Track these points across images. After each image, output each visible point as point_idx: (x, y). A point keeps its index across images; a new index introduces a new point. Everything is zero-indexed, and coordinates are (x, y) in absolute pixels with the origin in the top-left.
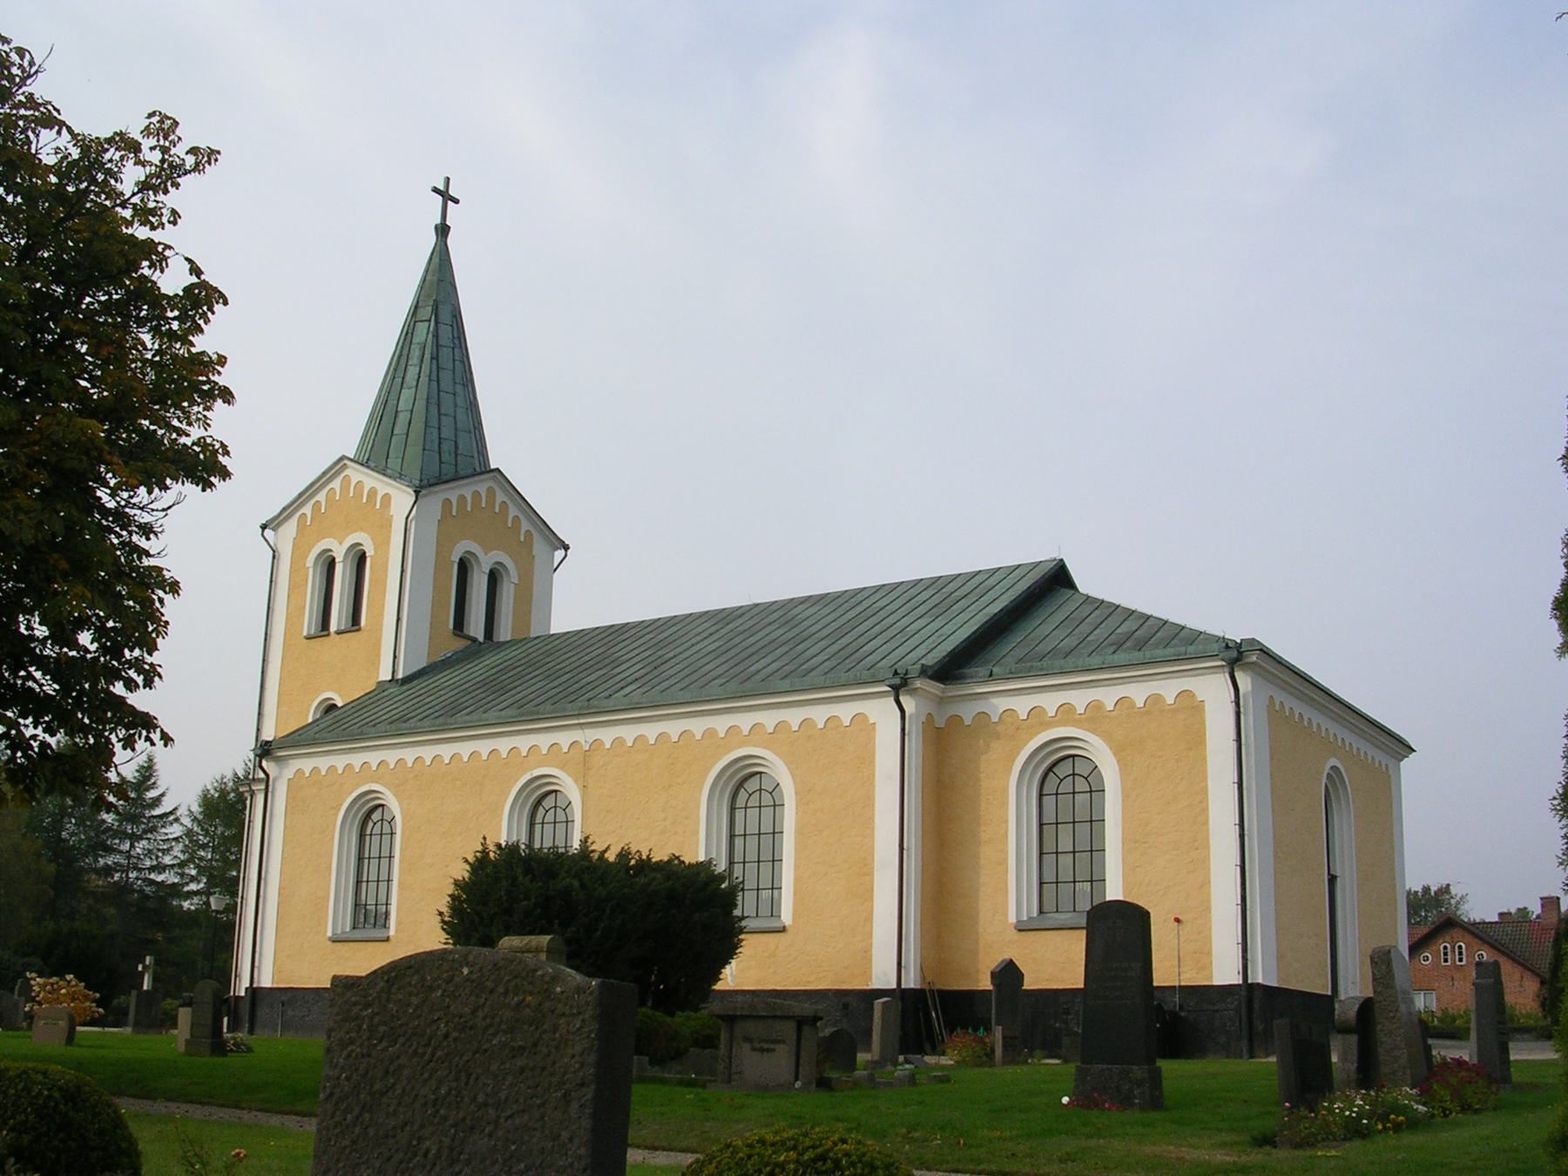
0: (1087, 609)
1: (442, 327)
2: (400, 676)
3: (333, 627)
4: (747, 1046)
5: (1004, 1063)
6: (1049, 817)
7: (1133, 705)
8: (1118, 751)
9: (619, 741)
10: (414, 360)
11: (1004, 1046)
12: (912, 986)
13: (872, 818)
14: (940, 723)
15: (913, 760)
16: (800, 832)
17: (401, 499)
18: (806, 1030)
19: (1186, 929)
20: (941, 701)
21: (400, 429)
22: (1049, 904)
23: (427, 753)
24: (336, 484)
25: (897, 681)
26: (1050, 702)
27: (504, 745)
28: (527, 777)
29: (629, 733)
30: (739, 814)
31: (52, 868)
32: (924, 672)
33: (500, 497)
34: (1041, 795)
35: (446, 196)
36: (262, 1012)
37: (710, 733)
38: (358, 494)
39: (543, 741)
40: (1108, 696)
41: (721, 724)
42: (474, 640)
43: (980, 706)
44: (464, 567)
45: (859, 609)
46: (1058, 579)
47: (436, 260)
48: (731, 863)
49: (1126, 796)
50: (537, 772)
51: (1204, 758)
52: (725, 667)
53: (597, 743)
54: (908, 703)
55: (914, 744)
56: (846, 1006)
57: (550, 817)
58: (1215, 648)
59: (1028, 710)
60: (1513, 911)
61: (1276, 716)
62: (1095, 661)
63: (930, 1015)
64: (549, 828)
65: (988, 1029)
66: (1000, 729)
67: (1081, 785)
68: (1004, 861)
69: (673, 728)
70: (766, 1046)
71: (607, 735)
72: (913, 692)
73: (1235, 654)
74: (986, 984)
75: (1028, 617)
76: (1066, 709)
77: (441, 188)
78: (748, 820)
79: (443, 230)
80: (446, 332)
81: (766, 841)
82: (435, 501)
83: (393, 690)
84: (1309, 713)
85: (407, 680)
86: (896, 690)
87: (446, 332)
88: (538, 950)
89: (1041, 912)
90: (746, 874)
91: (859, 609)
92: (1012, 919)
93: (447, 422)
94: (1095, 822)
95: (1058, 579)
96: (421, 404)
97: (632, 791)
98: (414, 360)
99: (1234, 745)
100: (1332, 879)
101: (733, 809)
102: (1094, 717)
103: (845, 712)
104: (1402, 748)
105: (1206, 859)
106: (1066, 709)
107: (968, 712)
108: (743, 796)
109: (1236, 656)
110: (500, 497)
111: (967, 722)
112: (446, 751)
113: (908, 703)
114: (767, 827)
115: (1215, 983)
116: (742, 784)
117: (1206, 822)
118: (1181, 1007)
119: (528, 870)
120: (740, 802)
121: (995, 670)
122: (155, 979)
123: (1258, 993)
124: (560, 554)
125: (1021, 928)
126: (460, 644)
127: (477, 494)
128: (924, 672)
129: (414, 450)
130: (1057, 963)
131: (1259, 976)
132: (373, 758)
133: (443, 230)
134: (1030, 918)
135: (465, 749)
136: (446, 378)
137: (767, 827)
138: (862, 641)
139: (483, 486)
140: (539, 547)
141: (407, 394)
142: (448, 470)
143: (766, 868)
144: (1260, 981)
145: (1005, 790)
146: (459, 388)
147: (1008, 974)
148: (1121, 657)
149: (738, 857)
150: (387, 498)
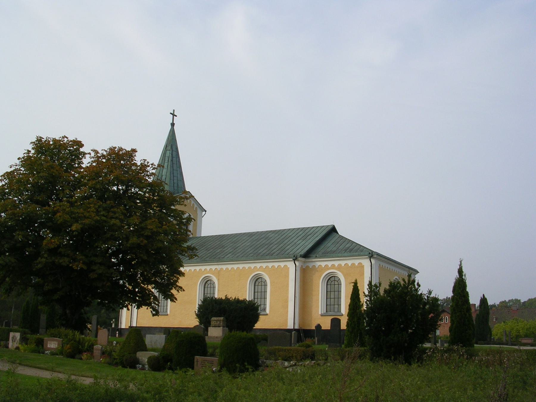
0: (339, 239)
6: (329, 290)
9: (227, 269)
15: (298, 277)
16: (271, 292)
20: (305, 262)
22: (328, 310)
26: (330, 264)
27: (198, 268)
28: (204, 276)
30: (256, 287)
34: (327, 285)
35: (174, 115)
37: (250, 268)
39: (208, 268)
40: (343, 263)
41: (252, 266)
45: (284, 236)
48: (254, 298)
50: (206, 275)
52: (253, 250)
53: (222, 269)
57: (209, 286)
59: (325, 265)
60: (507, 301)
61: (381, 268)
62: (340, 255)
63: (303, 334)
64: (209, 289)
65: (314, 338)
67: (336, 283)
69: (241, 266)
71: (224, 267)
72: (298, 260)
74: (314, 328)
76: (333, 266)
79: (173, 125)
81: (263, 293)
84: (389, 267)
86: (294, 260)
87: (174, 153)
88: (220, 320)
90: (258, 302)
91: (284, 236)
92: (320, 313)
93: (175, 178)
94: (339, 292)
95: (333, 230)
96: (168, 174)
99: (370, 276)
102: (339, 268)
103: (282, 264)
106: (333, 266)
107: (311, 265)
108: (257, 283)
114: (263, 290)
116: (258, 281)
119: (216, 303)
124: (204, 213)
125: (322, 315)
130: (326, 325)
133: (173, 125)
136: (175, 166)
137: (263, 290)
138: (286, 245)
143: (263, 300)
146: (178, 169)
147: (319, 327)
148: (346, 254)
149: (256, 297)
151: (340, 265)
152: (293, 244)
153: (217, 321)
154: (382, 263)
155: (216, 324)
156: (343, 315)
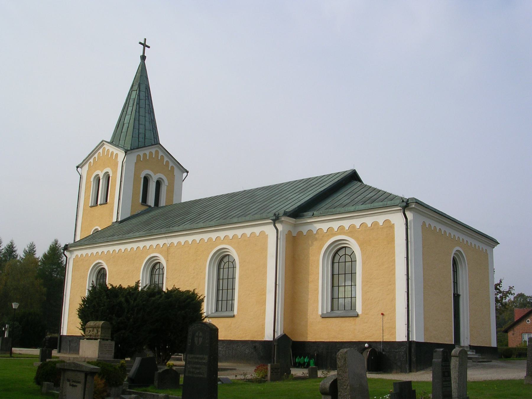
1: (141, 93)
2: (119, 220)
3: (99, 203)
4: (68, 383)
5: (272, 380)
7: (367, 226)
8: (361, 245)
10: (131, 105)
11: (271, 372)
13: (266, 273)
14: (294, 234)
17: (121, 154)
18: (89, 377)
19: (386, 318)
20: (295, 226)
21: (124, 130)
23: (117, 248)
24: (101, 151)
25: (274, 218)
26: (335, 225)
27: (141, 245)
29: (182, 240)
30: (336, 265)
31: (45, 289)
32: (286, 214)
33: (161, 154)
35: (144, 45)
36: (63, 344)
37: (210, 239)
38: (108, 154)
39: (154, 243)
40: (357, 222)
41: (213, 236)
42: (150, 206)
43: (309, 227)
44: (146, 180)
46: (353, 177)
47: (140, 68)
49: (364, 263)
50: (152, 255)
51: (394, 247)
54: (280, 226)
55: (282, 243)
56: (255, 347)
58: (398, 202)
59: (328, 228)
61: (425, 228)
66: (317, 236)
67: (348, 259)
68: (317, 289)
70: (75, 384)
71: (175, 241)
72: (281, 222)
73: (404, 204)
75: (341, 190)
76: (341, 228)
77: (143, 42)
78: (224, 273)
79: (143, 58)
80: (143, 94)
81: (230, 281)
82: (133, 156)
83: (116, 225)
85: (121, 222)
88: (98, 327)
89: (332, 309)
92: (320, 313)
93: (142, 127)
95: (353, 177)
96: (132, 121)
97: (181, 262)
98: (131, 105)
100: (457, 297)
101: (333, 263)
102: (352, 232)
103: (257, 230)
104: (494, 242)
105: (394, 290)
106: (341, 228)
107: (305, 230)
109: (406, 205)
110: (161, 154)
111: (315, 232)
112: (123, 247)
115: (397, 340)
116: (223, 261)
117: (394, 274)
118: (383, 350)
120: (336, 260)
121: (315, 213)
122: (9, 335)
124: (185, 174)
125: (323, 317)
126: (144, 208)
127: (151, 153)
128: (286, 214)
129: (129, 137)
131: (414, 338)
132: (100, 250)
133: (143, 58)
134: (327, 313)
135: (129, 247)
139: (153, 150)
140: (176, 171)
141: (128, 117)
142: (141, 144)
145: (318, 260)
146: (147, 115)
150: (117, 155)
151: (352, 227)
152: (285, 198)
153: (93, 328)
154: (428, 222)
155: (91, 333)
156: (358, 316)
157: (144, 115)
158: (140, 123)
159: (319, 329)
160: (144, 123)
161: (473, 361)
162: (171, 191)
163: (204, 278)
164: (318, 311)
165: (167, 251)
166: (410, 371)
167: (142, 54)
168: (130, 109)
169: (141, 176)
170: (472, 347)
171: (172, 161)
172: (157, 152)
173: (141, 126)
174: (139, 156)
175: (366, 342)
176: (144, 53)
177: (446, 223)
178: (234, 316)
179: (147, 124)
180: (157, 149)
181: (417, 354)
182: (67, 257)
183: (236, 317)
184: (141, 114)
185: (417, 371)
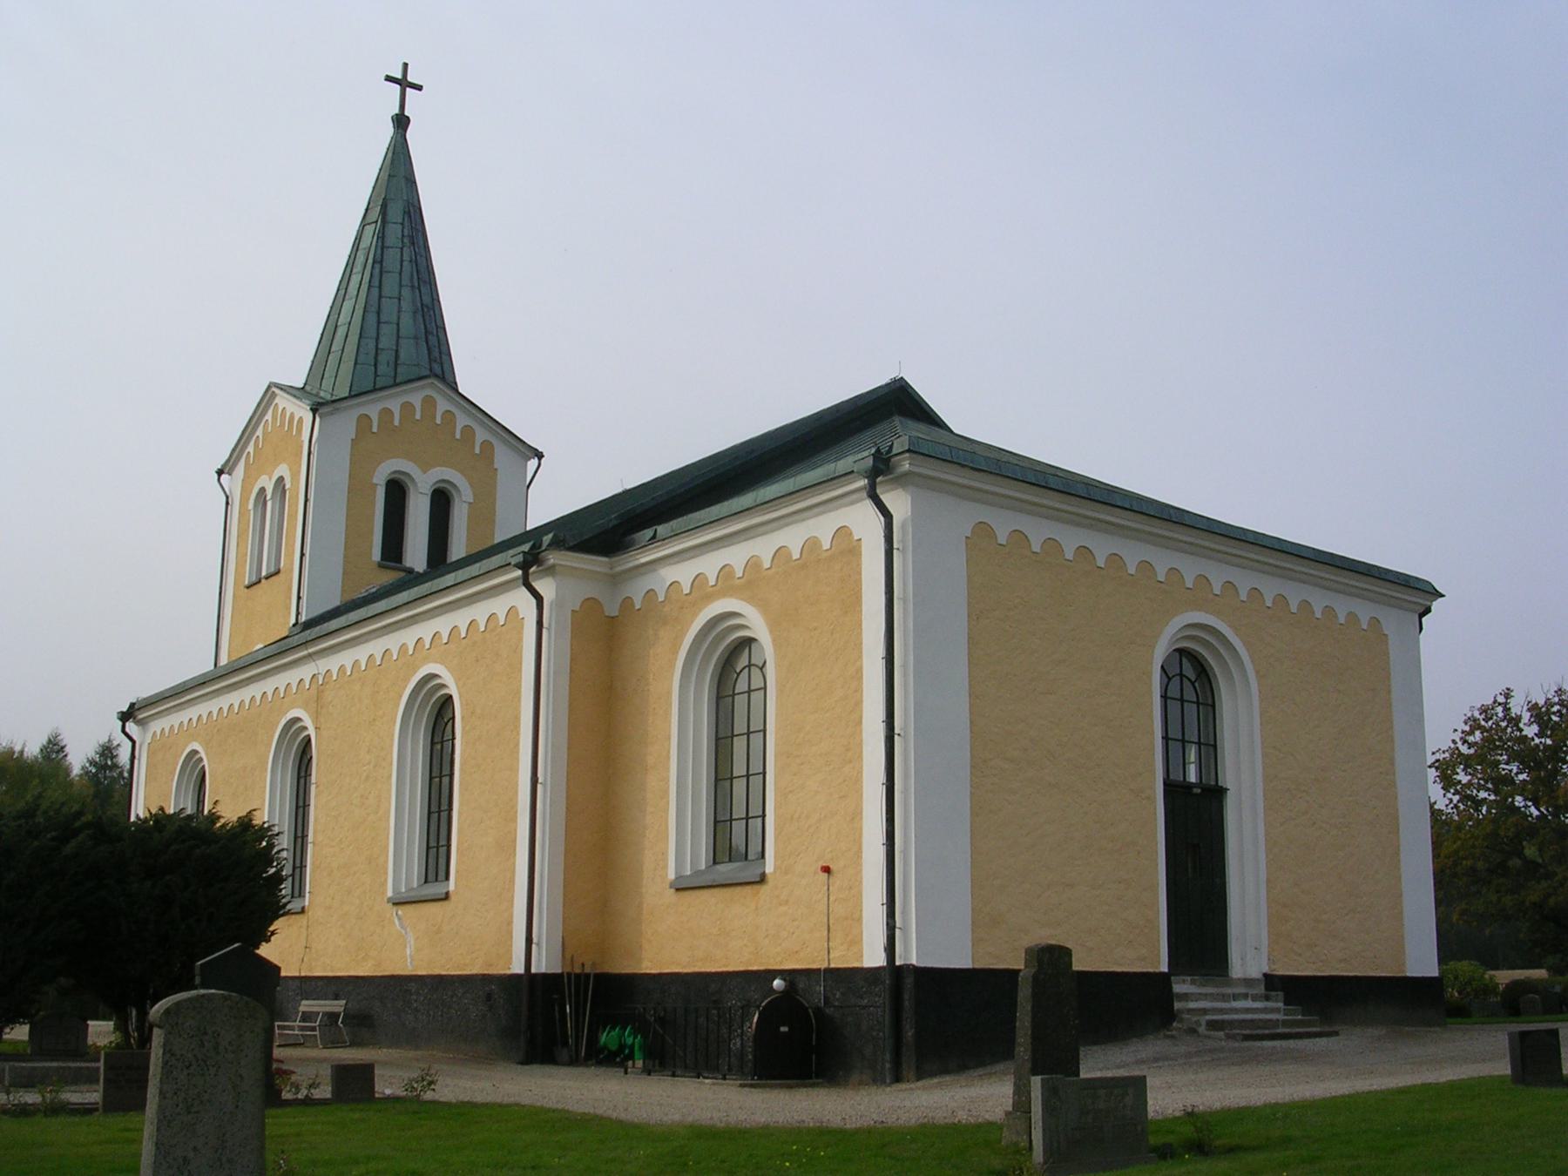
1: (390, 228)
2: (303, 618)
8: (773, 625)
12: (543, 970)
14: (612, 610)
19: (836, 881)
20: (616, 580)
28: (283, 722)
35: (403, 83)
42: (410, 571)
44: (397, 492)
46: (897, 402)
54: (545, 586)
77: (399, 76)
79: (401, 122)
80: (394, 232)
82: (346, 423)
92: (672, 876)
93: (387, 331)
102: (751, 583)
104: (1415, 595)
107: (636, 591)
113: (545, 586)
123: (909, 982)
124: (533, 463)
125: (681, 887)
126: (388, 577)
127: (407, 408)
129: (348, 366)
131: (911, 954)
133: (401, 122)
140: (503, 457)
141: (348, 305)
144: (914, 962)
145: (669, 693)
146: (406, 292)
154: (1004, 524)
157: (396, 294)
158: (384, 318)
159: (683, 934)
160: (395, 319)
161: (1228, 1037)
162: (484, 513)
163: (390, 776)
164: (666, 867)
165: (317, 696)
166: (898, 1079)
167: (397, 111)
168: (356, 279)
169: (375, 481)
170: (1272, 983)
171: (482, 424)
172: (429, 403)
173: (385, 329)
174: (364, 420)
175: (772, 974)
176: (402, 106)
177: (1122, 527)
178: (447, 897)
179: (407, 321)
180: (429, 392)
181: (935, 1016)
182: (134, 742)
183: (453, 898)
184: (386, 291)
185: (921, 1075)
